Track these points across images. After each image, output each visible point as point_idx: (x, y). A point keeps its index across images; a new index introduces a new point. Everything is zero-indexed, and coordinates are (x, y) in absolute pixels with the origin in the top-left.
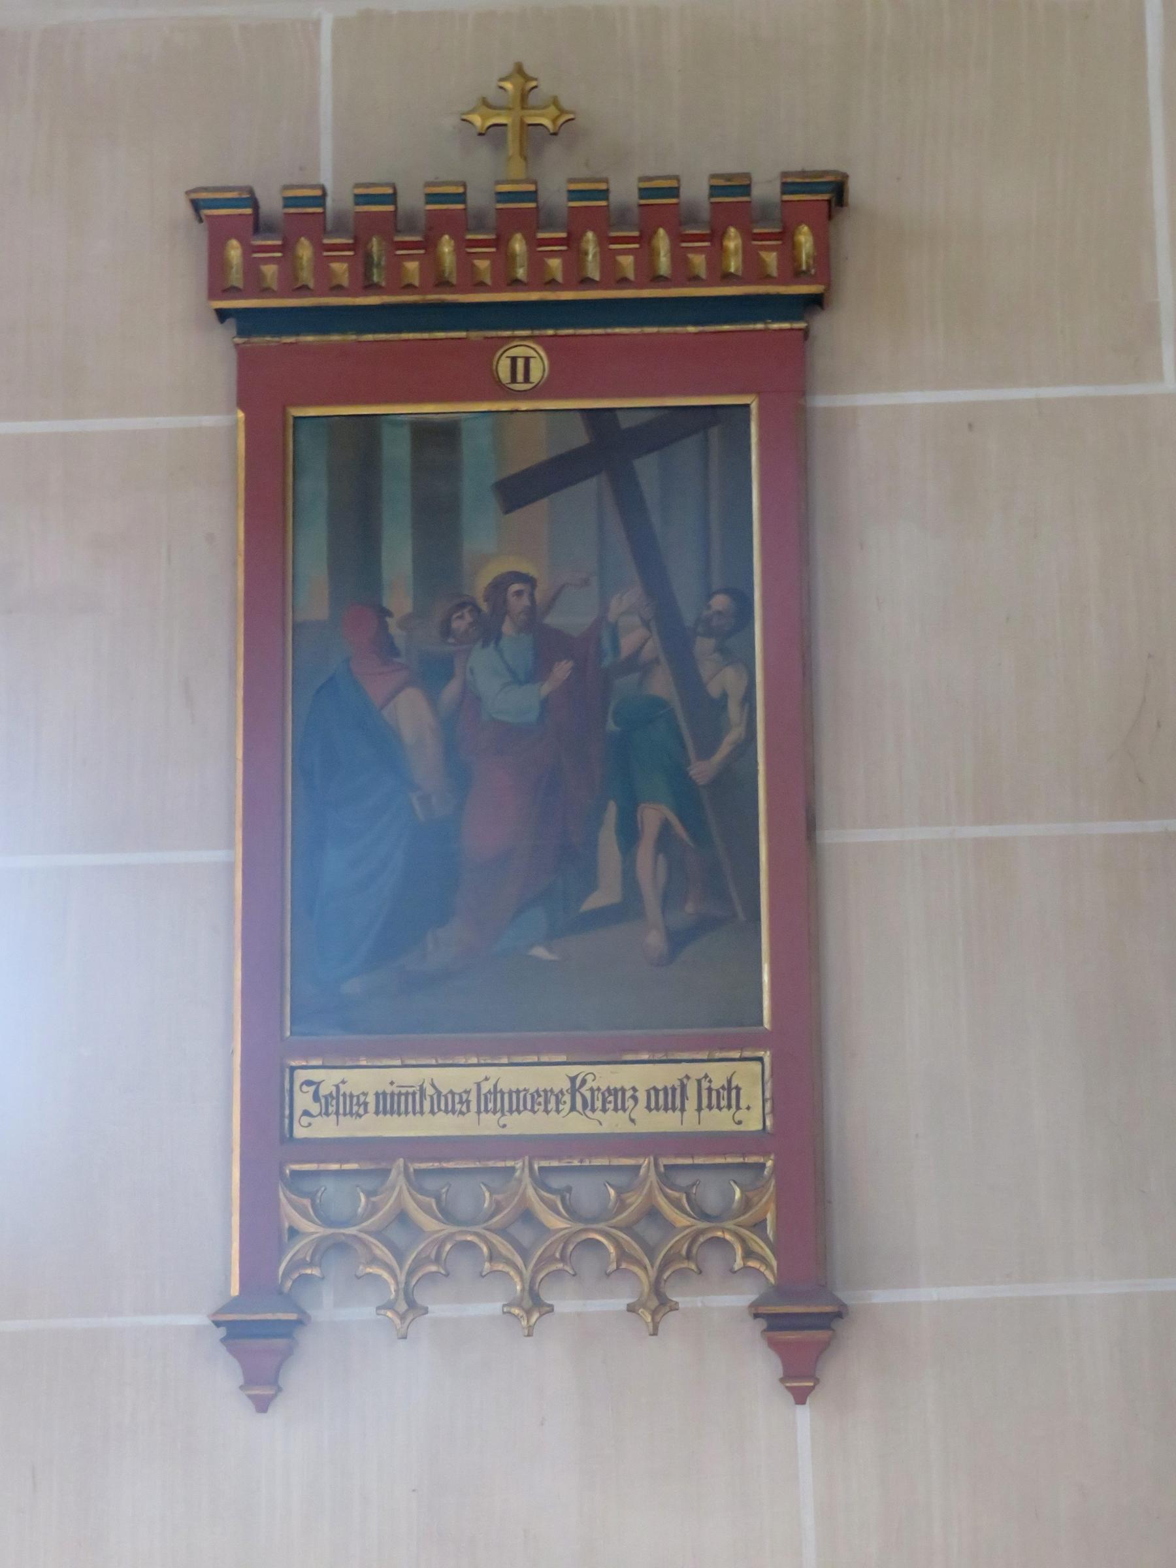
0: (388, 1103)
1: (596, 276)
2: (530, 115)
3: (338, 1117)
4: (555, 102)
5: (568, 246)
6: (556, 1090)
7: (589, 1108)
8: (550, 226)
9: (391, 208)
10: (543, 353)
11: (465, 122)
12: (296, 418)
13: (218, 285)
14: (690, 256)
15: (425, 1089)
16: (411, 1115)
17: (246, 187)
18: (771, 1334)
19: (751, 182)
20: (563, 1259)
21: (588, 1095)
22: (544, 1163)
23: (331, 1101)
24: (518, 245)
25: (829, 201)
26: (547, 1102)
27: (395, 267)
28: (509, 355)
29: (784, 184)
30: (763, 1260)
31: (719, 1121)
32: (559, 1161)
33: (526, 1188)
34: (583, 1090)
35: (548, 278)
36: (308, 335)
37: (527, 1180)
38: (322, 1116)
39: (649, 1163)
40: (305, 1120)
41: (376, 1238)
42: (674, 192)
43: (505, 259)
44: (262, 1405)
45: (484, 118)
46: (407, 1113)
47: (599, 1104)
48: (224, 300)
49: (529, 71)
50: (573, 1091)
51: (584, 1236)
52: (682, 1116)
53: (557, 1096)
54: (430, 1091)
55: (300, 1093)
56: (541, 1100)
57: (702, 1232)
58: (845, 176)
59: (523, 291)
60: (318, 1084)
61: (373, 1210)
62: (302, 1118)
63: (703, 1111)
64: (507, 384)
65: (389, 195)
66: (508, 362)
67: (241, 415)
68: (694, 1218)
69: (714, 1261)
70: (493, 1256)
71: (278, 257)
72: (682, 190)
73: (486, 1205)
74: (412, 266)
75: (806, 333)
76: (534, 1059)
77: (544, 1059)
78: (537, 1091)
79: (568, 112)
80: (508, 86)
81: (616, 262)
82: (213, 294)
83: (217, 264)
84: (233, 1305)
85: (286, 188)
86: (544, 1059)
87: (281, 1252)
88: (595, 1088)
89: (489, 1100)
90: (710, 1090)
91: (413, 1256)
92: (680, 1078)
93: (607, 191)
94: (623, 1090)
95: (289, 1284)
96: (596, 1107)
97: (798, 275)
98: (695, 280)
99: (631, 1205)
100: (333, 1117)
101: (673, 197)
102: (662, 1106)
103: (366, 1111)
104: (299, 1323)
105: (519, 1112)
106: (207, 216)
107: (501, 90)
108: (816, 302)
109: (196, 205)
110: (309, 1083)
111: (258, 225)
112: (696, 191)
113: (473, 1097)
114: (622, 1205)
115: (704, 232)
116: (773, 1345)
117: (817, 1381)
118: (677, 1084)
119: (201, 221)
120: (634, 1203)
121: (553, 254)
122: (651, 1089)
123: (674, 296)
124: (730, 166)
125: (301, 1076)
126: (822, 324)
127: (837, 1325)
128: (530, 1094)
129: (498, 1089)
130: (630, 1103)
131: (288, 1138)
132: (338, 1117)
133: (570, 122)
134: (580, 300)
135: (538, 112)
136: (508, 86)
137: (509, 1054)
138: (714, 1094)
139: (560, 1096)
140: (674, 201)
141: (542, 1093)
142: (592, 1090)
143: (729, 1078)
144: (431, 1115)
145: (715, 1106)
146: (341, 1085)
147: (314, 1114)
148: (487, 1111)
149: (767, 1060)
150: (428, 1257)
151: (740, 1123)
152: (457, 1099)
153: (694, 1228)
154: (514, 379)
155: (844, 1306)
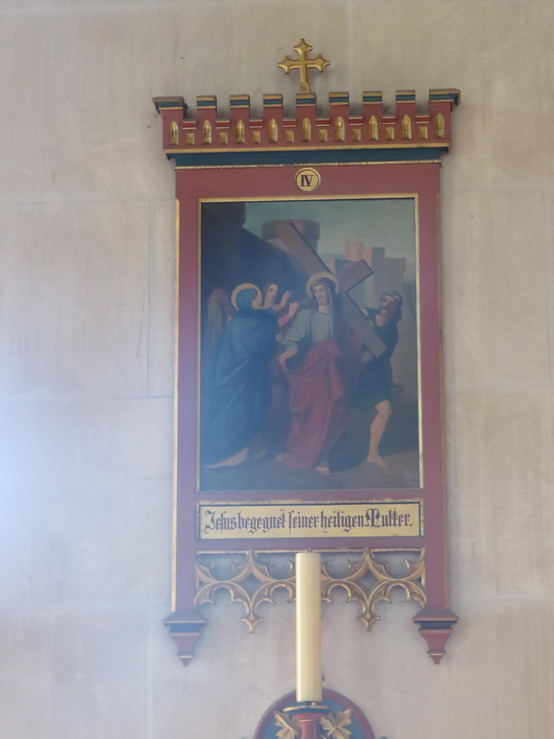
0: (278, 522)
1: (343, 138)
4: (320, 57)
8: (255, 117)
9: (214, 107)
10: (317, 172)
12: (202, 203)
13: (168, 143)
20: (268, 596)
22: (259, 552)
24: (340, 122)
25: (451, 103)
36: (187, 166)
37: (251, 559)
40: (208, 529)
42: (380, 98)
43: (201, 133)
44: (437, 660)
46: (390, 525)
48: (435, 143)
49: (307, 41)
51: (397, 584)
52: (290, 530)
56: (313, 521)
57: (391, 583)
65: (213, 101)
66: (301, 177)
67: (178, 202)
72: (383, 97)
74: (191, 135)
75: (440, 165)
76: (226, 503)
77: (230, 503)
78: (260, 518)
81: (219, 136)
83: (167, 134)
85: (364, 92)
86: (230, 503)
90: (342, 517)
91: (257, 593)
92: (238, 513)
93: (381, 97)
97: (438, 139)
98: (389, 141)
99: (417, 569)
103: (235, 526)
104: (204, 625)
106: (162, 110)
108: (445, 150)
110: (209, 512)
111: (186, 113)
112: (389, 99)
118: (388, 514)
119: (159, 112)
120: (419, 568)
121: (391, 126)
122: (252, 519)
124: (407, 86)
125: (204, 509)
126: (445, 160)
127: (453, 626)
128: (341, 517)
129: (324, 516)
133: (328, 66)
137: (331, 500)
141: (262, 520)
146: (292, 513)
149: (421, 503)
150: (206, 595)
153: (270, 583)
154: (303, 185)
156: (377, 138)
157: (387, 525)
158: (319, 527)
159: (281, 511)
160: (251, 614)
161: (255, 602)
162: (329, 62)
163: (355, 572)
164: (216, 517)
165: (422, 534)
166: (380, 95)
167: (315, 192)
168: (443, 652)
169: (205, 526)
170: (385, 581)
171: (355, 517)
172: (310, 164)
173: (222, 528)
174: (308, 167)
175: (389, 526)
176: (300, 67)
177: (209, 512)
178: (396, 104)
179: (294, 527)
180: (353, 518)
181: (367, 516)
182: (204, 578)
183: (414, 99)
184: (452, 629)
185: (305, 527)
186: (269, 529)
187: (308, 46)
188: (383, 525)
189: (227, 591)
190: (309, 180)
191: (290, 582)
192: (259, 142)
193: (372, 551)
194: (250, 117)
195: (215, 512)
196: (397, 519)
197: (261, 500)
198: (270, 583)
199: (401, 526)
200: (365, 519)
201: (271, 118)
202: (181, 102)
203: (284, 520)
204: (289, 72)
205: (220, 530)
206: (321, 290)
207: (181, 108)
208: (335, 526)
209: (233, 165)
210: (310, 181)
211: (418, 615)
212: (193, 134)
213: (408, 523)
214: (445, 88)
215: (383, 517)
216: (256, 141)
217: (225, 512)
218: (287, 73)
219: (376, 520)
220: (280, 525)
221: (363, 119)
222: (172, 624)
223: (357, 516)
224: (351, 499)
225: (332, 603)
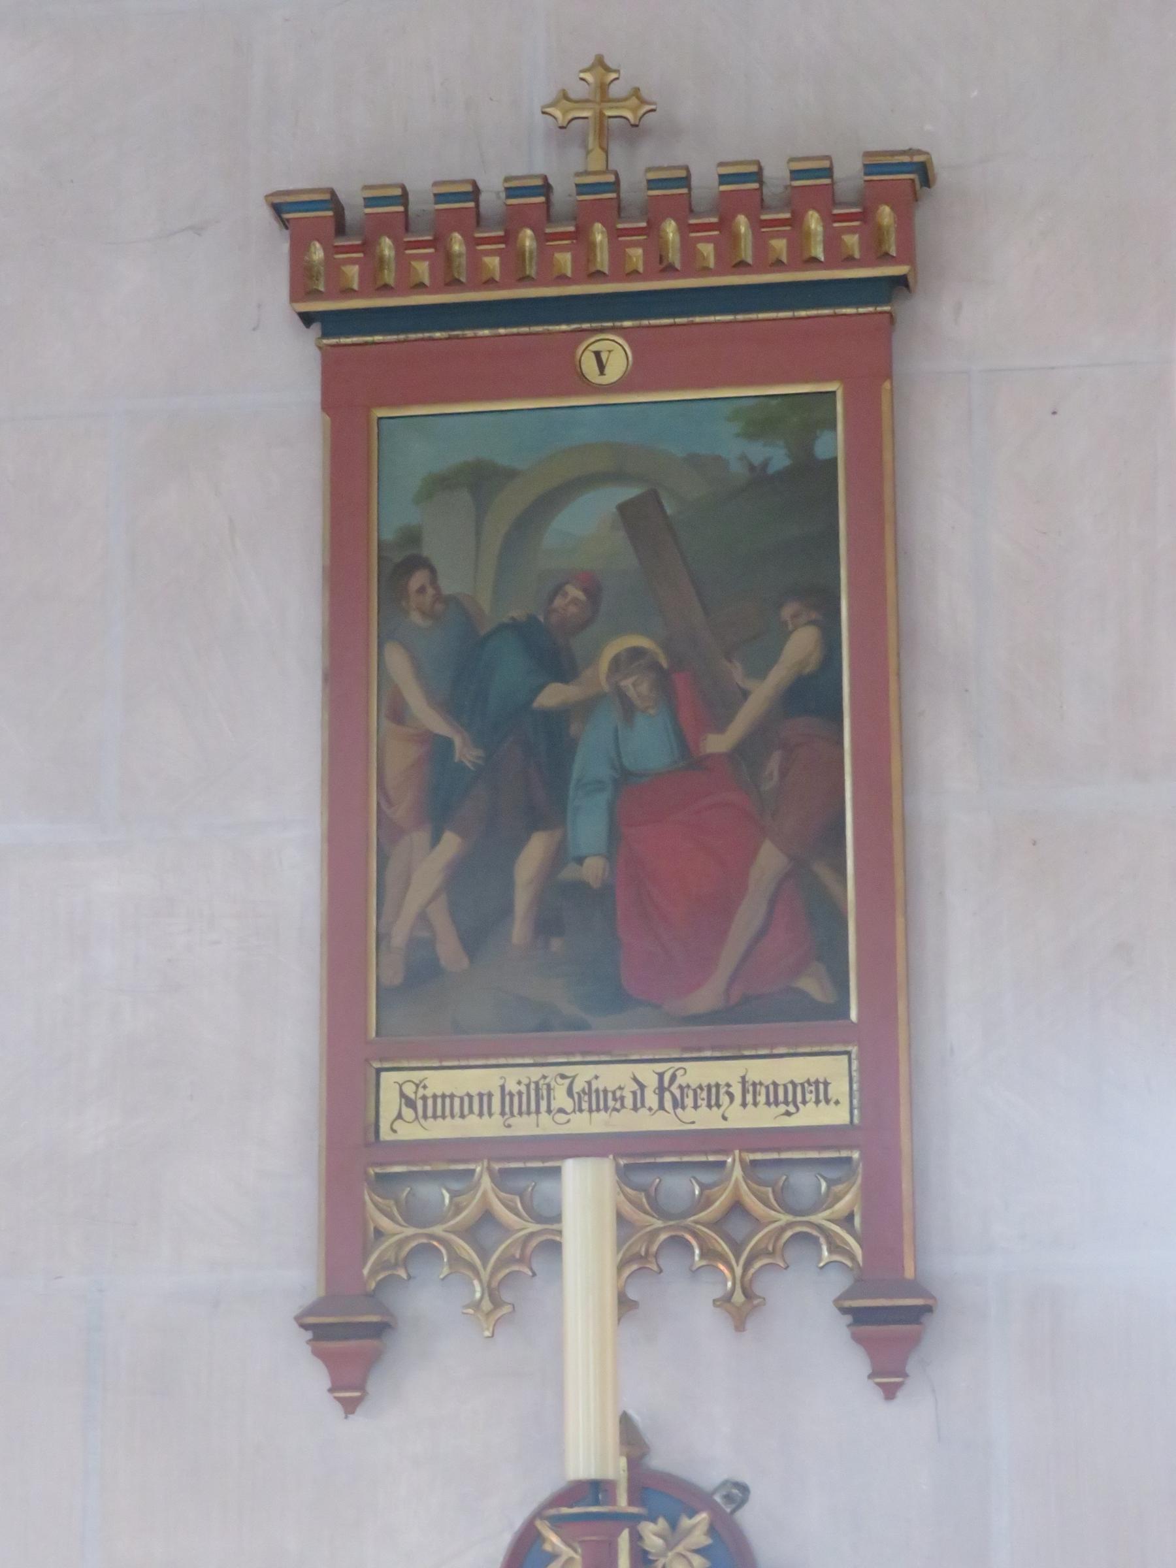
4: (636, 92)
6: (694, 1086)
7: (680, 1106)
11: (546, 116)
14: (414, 263)
16: (823, 1104)
17: (328, 189)
21: (677, 1093)
24: (599, 235)
27: (332, 267)
31: (810, 1116)
32: (543, 1163)
35: (485, 278)
38: (575, 1113)
39: (734, 1160)
43: (373, 265)
44: (890, 1392)
45: (565, 113)
47: (689, 1101)
50: (661, 1090)
51: (798, 1229)
55: (558, 1086)
59: (750, 273)
60: (574, 1077)
61: (458, 1209)
63: (540, 1115)
66: (593, 356)
70: (456, 1259)
71: (715, 235)
75: (891, 317)
76: (437, 1064)
80: (588, 76)
82: (294, 297)
84: (311, 1311)
85: (507, 179)
87: (366, 1254)
88: (684, 1085)
89: (685, 1095)
94: (718, 1086)
95: (373, 1285)
97: (885, 258)
103: (623, 1106)
105: (462, 1116)
109: (278, 209)
110: (563, 1077)
113: (737, 1090)
117: (905, 1375)
122: (788, 1083)
123: (621, 291)
126: (903, 309)
129: (507, 1091)
130: (725, 1099)
134: (522, 299)
135: (618, 104)
136: (588, 76)
138: (799, 1090)
142: (681, 1087)
145: (459, 1114)
147: (569, 1111)
149: (853, 1056)
151: (509, 1126)
152: (610, 1096)
156: (822, 257)
158: (497, 1117)
159: (501, 1078)
163: (709, 1203)
165: (856, 1121)
166: (719, 169)
167: (624, 385)
171: (701, 1087)
173: (590, 1111)
177: (563, 1077)
182: (385, 1223)
184: (920, 1323)
186: (798, 1109)
189: (815, 1241)
190: (604, 360)
192: (641, 270)
194: (835, 204)
197: (765, 1046)
198: (649, 1229)
201: (592, 223)
202: (333, 202)
204: (637, 123)
205: (586, 1114)
206: (575, 601)
207: (330, 213)
208: (768, 1103)
209: (857, 308)
210: (607, 362)
212: (640, 251)
216: (599, 267)
218: (562, 127)
221: (364, 244)
223: (704, 1084)
224: (584, 1053)
225: (691, 1271)
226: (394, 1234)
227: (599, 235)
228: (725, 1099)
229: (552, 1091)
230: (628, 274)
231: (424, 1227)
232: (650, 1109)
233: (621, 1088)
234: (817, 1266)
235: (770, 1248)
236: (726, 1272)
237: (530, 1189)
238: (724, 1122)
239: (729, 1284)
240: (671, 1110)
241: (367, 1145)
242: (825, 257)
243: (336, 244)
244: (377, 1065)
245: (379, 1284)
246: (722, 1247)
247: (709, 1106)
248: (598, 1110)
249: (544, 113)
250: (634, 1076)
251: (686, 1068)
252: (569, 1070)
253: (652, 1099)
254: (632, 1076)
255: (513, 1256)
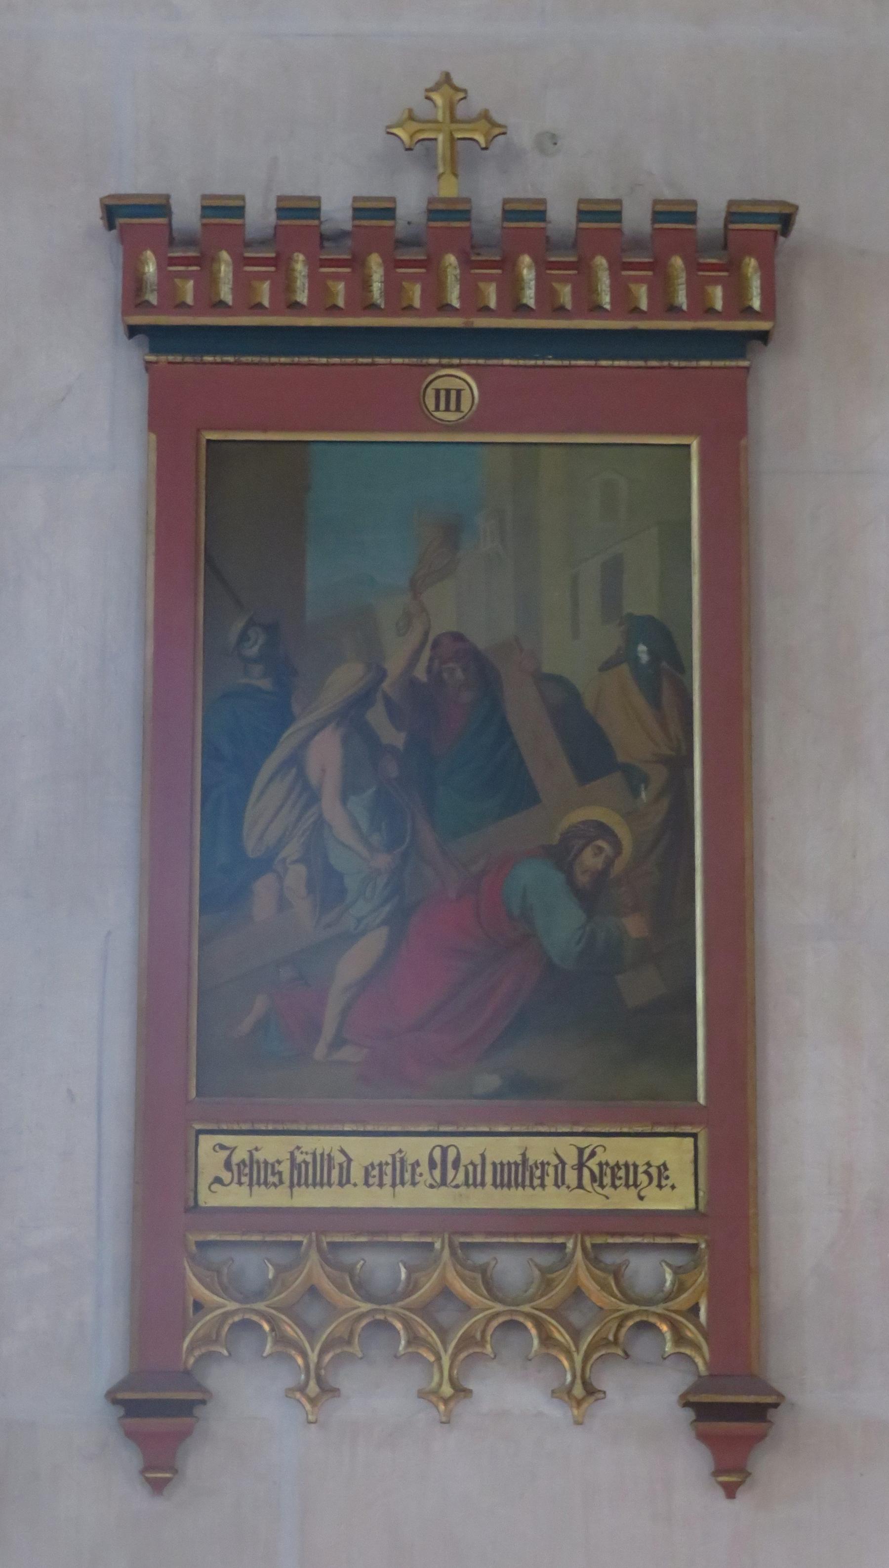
2: (459, 130)
3: (251, 1190)
5: (200, 267)
6: (612, 1163)
11: (390, 136)
12: (208, 441)
14: (330, 283)
15: (334, 1157)
18: (129, 1421)
19: (622, 209)
21: (596, 1170)
23: (244, 1169)
26: (381, 1174)
28: (434, 387)
29: (355, 210)
30: (697, 1347)
33: (576, 1270)
34: (589, 1164)
35: (405, 304)
41: (550, 1316)
44: (730, 1491)
46: (517, 1185)
47: (607, 1180)
49: (457, 81)
53: (612, 1169)
54: (339, 1158)
56: (376, 1172)
58: (796, 208)
60: (233, 1150)
62: (227, 1184)
63: (396, 1188)
64: (433, 411)
68: (620, 1300)
69: (643, 1346)
70: (281, 1339)
71: (725, 276)
73: (668, 1284)
76: (648, 1129)
78: (536, 1163)
79: (500, 126)
82: (125, 312)
84: (124, 1385)
88: (604, 1162)
93: (619, 213)
95: (192, 1361)
96: (332, 1182)
100: (388, 1189)
101: (313, 218)
102: (408, 1181)
103: (281, 1182)
107: (428, 101)
108: (764, 337)
110: (222, 1147)
113: (285, 1168)
114: (412, 1286)
115: (646, 260)
116: (703, 1437)
118: (519, 1159)
121: (337, 277)
122: (302, 1162)
129: (255, 1160)
131: (194, 1208)
132: (251, 1190)
139: (616, 1170)
140: (691, 227)
141: (539, 1166)
143: (554, 1152)
144: (365, 1187)
145: (337, 1182)
146: (254, 1152)
148: (403, 1183)
154: (437, 408)
155: (781, 1396)
157: (322, 1185)
160: (312, 1384)
161: (458, 1350)
162: (505, 127)
164: (235, 1159)
165: (702, 1207)
168: (175, 1471)
169: (214, 1175)
170: (619, 1310)
172: (456, 361)
174: (451, 366)
175: (520, 1188)
176: (441, 138)
178: (503, 228)
179: (403, 1183)
180: (659, 1168)
181: (432, 1164)
183: (619, 221)
185: (304, 1186)
187: (457, 89)
188: (467, 1184)
191: (537, 1312)
193: (325, 1240)
195: (235, 1148)
196: (407, 1171)
199: (618, 1189)
200: (424, 1168)
203: (546, 1173)
211: (695, 1389)
213: (664, 1182)
214: (766, 197)
215: (494, 1164)
216: (258, 300)
217: (257, 1149)
219: (451, 1173)
220: (537, 1182)
222: (131, 1401)
225: (493, 1359)
226: (483, 1310)
227: (300, 266)
228: (643, 1178)
229: (332, 1162)
230: (404, 309)
231: (380, 1304)
232: (568, 1187)
233: (279, 1162)
234: (262, 1356)
235: (611, 1338)
236: (566, 1364)
237: (624, 1267)
238: (639, 1201)
239: (569, 1378)
240: (589, 1188)
241: (187, 1210)
242: (158, 301)
243: (247, 255)
244: (198, 1127)
245: (197, 1361)
246: (432, 1338)
247: (556, 1185)
248: (299, 1185)
249: (388, 133)
250: (556, 1152)
251: (606, 1147)
252: (228, 1140)
253: (571, 1176)
254: (339, 1149)
255: (606, 1338)
